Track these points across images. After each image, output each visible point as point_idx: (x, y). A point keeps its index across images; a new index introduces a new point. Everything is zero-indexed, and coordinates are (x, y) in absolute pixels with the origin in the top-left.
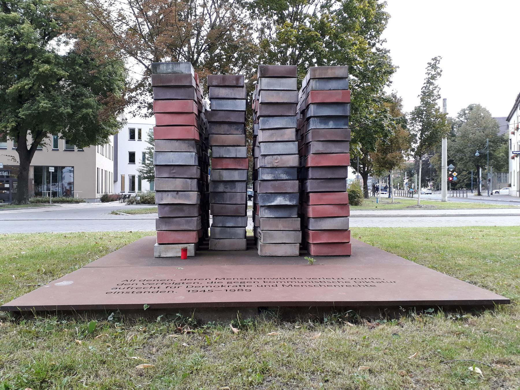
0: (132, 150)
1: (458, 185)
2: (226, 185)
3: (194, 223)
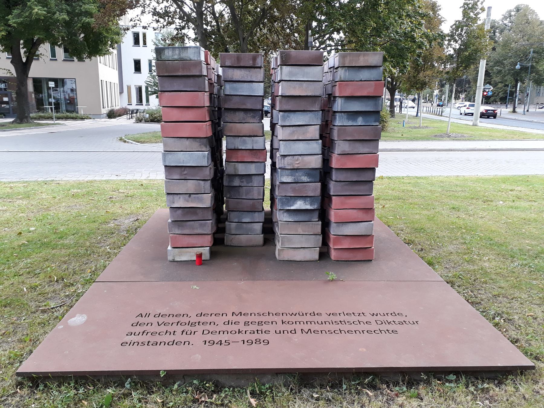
0: (137, 58)
1: (492, 99)
2: (242, 179)
3: (209, 226)
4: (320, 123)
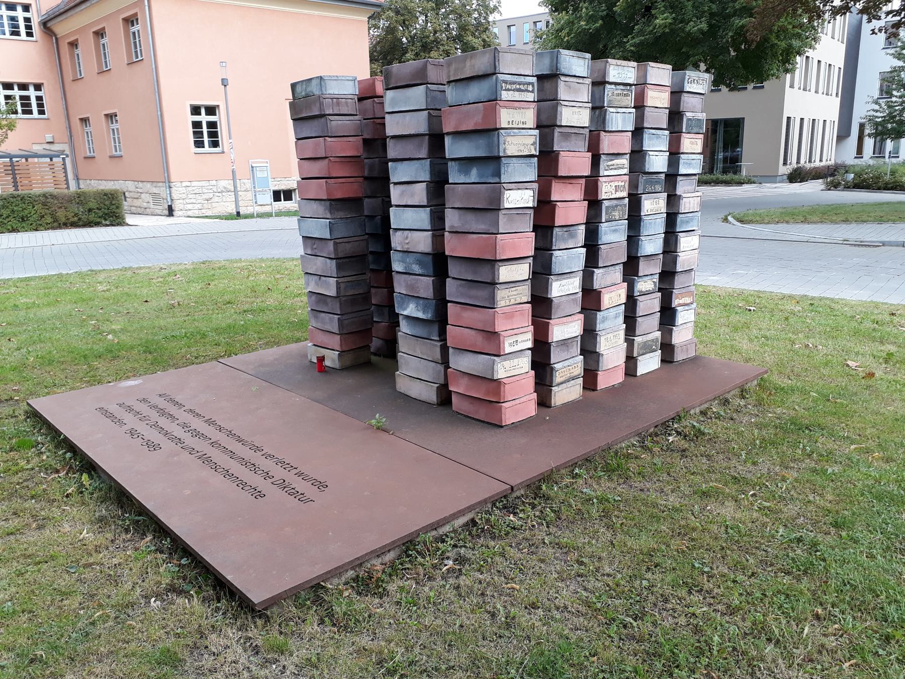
4: (428, 178)
